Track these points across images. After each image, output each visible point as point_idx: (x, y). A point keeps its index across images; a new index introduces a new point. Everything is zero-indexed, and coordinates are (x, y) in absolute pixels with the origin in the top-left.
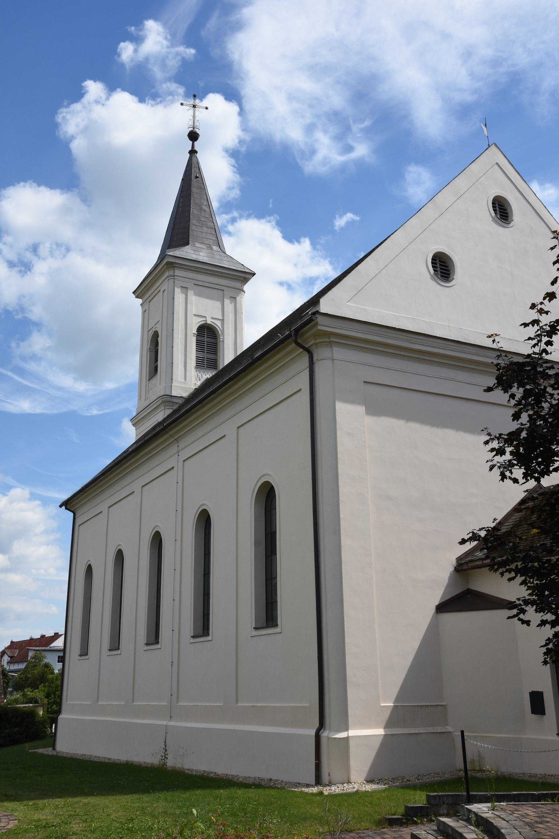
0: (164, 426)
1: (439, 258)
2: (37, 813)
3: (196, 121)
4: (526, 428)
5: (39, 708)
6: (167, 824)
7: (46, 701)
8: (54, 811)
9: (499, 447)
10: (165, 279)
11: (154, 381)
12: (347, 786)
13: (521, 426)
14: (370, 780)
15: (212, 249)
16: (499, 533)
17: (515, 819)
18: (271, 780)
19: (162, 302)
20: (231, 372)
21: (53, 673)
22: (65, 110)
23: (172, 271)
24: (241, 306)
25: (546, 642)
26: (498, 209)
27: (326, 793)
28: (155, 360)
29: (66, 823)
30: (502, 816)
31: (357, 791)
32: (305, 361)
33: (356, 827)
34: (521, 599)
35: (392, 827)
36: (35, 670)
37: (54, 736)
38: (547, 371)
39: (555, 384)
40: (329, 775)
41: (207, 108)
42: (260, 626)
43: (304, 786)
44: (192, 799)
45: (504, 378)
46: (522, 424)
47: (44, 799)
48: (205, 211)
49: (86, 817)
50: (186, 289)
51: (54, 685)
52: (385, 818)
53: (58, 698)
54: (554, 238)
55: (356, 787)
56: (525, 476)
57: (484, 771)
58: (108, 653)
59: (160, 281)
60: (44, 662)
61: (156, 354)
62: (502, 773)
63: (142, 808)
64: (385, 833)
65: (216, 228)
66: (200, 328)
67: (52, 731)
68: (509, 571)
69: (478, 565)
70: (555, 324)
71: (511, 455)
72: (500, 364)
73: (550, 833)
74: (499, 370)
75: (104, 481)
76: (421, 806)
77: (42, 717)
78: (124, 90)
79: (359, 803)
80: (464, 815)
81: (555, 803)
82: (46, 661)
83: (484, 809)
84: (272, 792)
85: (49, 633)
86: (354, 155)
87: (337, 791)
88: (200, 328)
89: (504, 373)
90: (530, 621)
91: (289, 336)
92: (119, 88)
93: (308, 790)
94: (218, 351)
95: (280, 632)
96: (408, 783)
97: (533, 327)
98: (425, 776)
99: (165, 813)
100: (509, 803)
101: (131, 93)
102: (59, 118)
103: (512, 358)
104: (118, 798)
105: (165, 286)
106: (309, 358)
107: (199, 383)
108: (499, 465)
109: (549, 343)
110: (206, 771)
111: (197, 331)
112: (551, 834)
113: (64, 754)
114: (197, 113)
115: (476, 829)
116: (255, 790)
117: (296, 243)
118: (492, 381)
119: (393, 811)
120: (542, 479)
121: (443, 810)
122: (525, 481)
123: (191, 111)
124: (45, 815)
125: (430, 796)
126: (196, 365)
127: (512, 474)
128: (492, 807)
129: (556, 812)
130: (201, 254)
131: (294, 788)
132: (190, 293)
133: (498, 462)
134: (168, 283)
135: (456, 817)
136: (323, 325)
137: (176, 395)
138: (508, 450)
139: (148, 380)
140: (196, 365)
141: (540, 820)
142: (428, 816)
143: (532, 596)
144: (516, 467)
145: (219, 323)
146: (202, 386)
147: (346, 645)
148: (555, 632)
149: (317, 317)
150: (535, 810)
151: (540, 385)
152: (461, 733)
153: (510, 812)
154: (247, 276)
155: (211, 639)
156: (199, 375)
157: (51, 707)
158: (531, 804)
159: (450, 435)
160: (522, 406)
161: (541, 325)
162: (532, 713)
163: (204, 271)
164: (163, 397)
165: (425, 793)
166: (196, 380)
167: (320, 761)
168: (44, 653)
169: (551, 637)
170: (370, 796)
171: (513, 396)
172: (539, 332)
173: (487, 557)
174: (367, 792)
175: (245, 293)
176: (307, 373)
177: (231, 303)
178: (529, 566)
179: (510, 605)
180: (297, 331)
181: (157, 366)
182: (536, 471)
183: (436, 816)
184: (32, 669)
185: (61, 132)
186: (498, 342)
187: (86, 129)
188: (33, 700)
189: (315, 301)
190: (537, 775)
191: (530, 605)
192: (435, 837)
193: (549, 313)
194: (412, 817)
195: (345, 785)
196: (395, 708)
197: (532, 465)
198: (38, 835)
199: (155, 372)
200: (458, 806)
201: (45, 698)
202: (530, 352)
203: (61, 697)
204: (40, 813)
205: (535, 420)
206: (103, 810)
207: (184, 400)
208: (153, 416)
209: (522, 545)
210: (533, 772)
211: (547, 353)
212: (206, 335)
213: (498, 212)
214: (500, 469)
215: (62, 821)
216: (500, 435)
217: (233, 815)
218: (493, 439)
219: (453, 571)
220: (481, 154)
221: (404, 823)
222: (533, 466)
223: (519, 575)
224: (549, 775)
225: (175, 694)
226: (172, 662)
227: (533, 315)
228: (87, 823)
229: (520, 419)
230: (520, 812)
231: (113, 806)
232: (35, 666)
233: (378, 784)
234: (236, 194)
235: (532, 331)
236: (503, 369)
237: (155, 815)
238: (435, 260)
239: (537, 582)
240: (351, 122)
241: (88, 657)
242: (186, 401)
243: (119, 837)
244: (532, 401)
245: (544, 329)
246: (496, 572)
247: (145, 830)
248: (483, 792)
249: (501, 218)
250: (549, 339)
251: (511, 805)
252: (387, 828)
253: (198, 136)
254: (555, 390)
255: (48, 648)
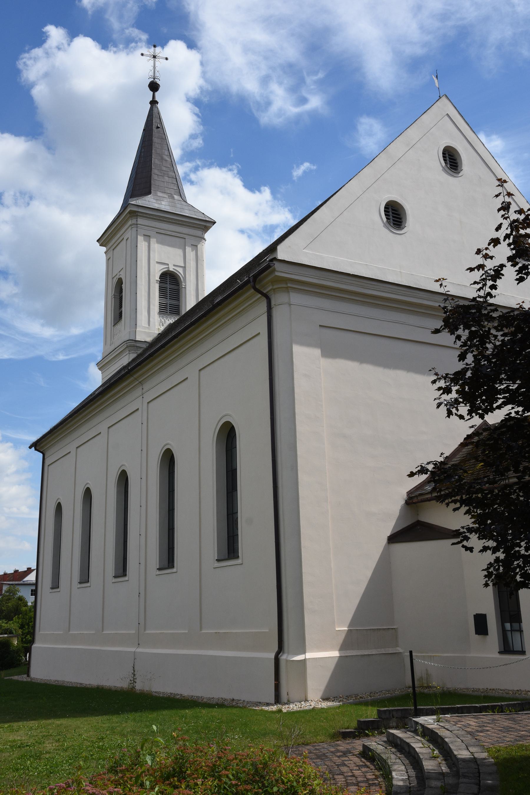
0: (128, 370)
1: (392, 207)
2: (12, 734)
3: (156, 71)
4: (471, 368)
5: (14, 638)
6: (135, 742)
7: (20, 632)
8: (29, 732)
9: (446, 386)
10: (129, 227)
11: (119, 326)
12: (304, 704)
13: (466, 366)
14: (325, 698)
15: (173, 198)
16: (447, 466)
17: (458, 729)
18: (233, 700)
19: (125, 251)
20: (192, 317)
21: (26, 605)
22: (26, 55)
23: (135, 220)
24: (202, 253)
25: (488, 566)
26: (448, 159)
27: (284, 710)
28: (120, 306)
29: (40, 743)
30: (446, 727)
31: (313, 709)
32: (263, 307)
33: (312, 741)
34: (465, 527)
35: (346, 740)
36: (9, 603)
37: (28, 664)
38: (491, 314)
39: (498, 326)
40: (288, 695)
41: (167, 59)
42: (223, 558)
43: (264, 705)
44: (159, 719)
45: (451, 320)
46: (467, 364)
47: (19, 721)
48: (166, 160)
49: (59, 737)
50: (148, 237)
51: (27, 616)
52: (339, 732)
53: (32, 629)
54: (499, 185)
55: (313, 705)
56: (470, 413)
57: (431, 687)
58: (78, 585)
59: (123, 230)
60: (18, 596)
61: (120, 300)
62: (447, 688)
63: (112, 728)
64: (339, 745)
65: (177, 177)
66: (163, 275)
67: (26, 659)
68: (455, 502)
69: (427, 498)
70: (499, 269)
71: (457, 393)
72: (447, 307)
73: (489, 741)
74: (445, 312)
75: (71, 423)
76: (372, 720)
77: (17, 647)
78: (86, 35)
79: (315, 719)
80: (412, 727)
81: (495, 714)
82: (19, 594)
83: (430, 721)
84: (234, 711)
85: (22, 568)
86: (308, 107)
87: (295, 708)
88: (163, 275)
89: (450, 316)
90: (473, 548)
91: (247, 282)
92: (81, 34)
93: (268, 708)
94: (181, 297)
95: (241, 563)
96: (361, 699)
97: (479, 271)
98: (377, 693)
99: (134, 732)
100: (453, 715)
101: (94, 40)
102: (20, 65)
103: (458, 301)
104: (89, 719)
105: (128, 235)
106: (267, 303)
107: (162, 328)
108: (446, 403)
109: (493, 287)
110: (172, 693)
111: (160, 278)
112: (491, 741)
113: (38, 681)
114: (157, 64)
115: (422, 739)
116: (218, 710)
117: (257, 192)
118: (439, 324)
119: (346, 725)
120: (486, 416)
121: (392, 723)
122: (470, 417)
123: (151, 62)
124: (20, 736)
125: (381, 711)
126: (159, 311)
127: (458, 411)
128: (437, 719)
129: (496, 722)
130: (163, 203)
131: (255, 707)
132: (153, 241)
133: (445, 400)
134: (131, 232)
135: (404, 729)
136: (280, 271)
137: (140, 340)
138: (454, 388)
139: (113, 325)
140: (159, 311)
141: (481, 729)
142: (379, 729)
143: (476, 524)
144: (461, 405)
145: (181, 270)
146: (166, 331)
147: (303, 575)
148: (496, 557)
149: (275, 264)
150: (476, 721)
151: (484, 327)
152: (410, 653)
153: (453, 723)
154: (208, 225)
155: (176, 571)
156: (162, 320)
157: (25, 637)
158: (473, 715)
159: (401, 375)
160: (467, 347)
161: (486, 269)
162: (476, 634)
163: (166, 220)
164: (127, 342)
165: (376, 708)
166: (160, 325)
167: (279, 682)
168: (17, 587)
169: (493, 562)
170: (326, 712)
171: (459, 337)
172: (484, 277)
173: (434, 490)
174: (322, 709)
175: (205, 241)
176: (265, 318)
177: (192, 251)
178: (473, 497)
179: (456, 534)
180: (255, 277)
181: (122, 312)
182: (480, 408)
183: (386, 729)
184: (7, 602)
185: (23, 80)
186: (445, 286)
187: (46, 75)
188: (7, 631)
189: (272, 248)
190: (479, 689)
191: (474, 533)
192: (385, 747)
193: (494, 258)
194: (364, 730)
195: (303, 703)
196: (349, 632)
197: (477, 403)
198: (13, 754)
199: (120, 317)
200: (406, 719)
201: (19, 629)
202: (475, 295)
203: (34, 627)
204: (15, 734)
205: (480, 360)
206: (75, 730)
207: (148, 345)
208: (117, 360)
209: (468, 478)
210: (476, 687)
211: (491, 296)
212: (168, 282)
213: (448, 162)
214: (447, 407)
215: (36, 741)
216: (447, 374)
217: (197, 732)
218: (440, 379)
219: (403, 504)
220: (432, 106)
221: (357, 736)
222: (478, 404)
223: (464, 505)
224: (490, 689)
225: (142, 622)
226: (139, 593)
227: (479, 260)
228: (59, 742)
229: (466, 360)
230: (463, 723)
231: (84, 727)
232: (10, 599)
233: (333, 701)
234: (199, 143)
235: (477, 275)
236: (450, 312)
237: (124, 734)
238: (388, 208)
239: (480, 511)
240: (305, 73)
241: (59, 589)
242: (150, 345)
243: (90, 754)
244: (476, 342)
245: (489, 273)
246: (442, 503)
247: (115, 748)
248: (430, 706)
249: (451, 168)
250: (494, 283)
251: (454, 716)
252: (341, 741)
253: (158, 87)
254: (499, 332)
255: (21, 582)
